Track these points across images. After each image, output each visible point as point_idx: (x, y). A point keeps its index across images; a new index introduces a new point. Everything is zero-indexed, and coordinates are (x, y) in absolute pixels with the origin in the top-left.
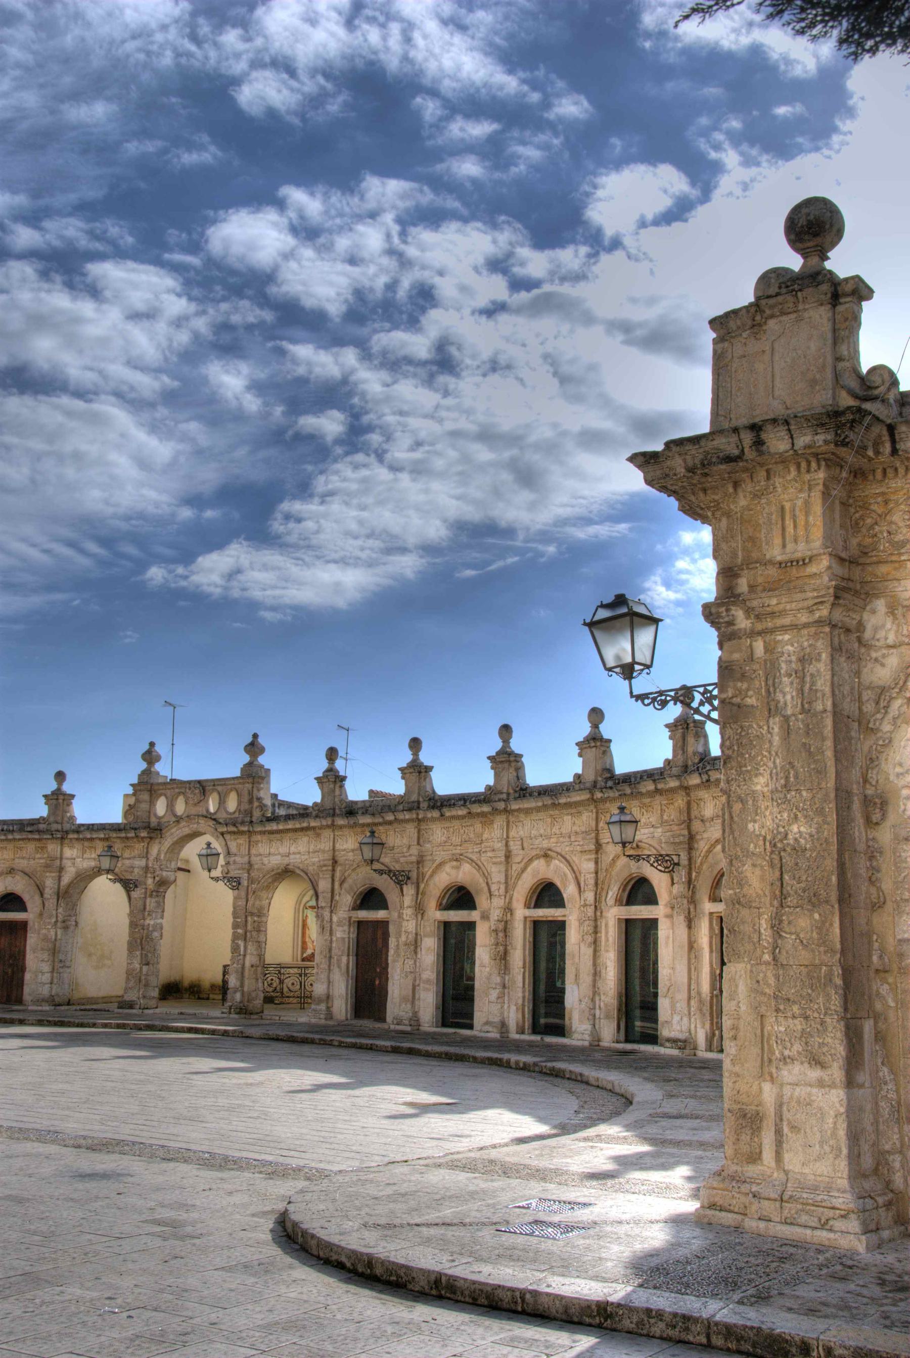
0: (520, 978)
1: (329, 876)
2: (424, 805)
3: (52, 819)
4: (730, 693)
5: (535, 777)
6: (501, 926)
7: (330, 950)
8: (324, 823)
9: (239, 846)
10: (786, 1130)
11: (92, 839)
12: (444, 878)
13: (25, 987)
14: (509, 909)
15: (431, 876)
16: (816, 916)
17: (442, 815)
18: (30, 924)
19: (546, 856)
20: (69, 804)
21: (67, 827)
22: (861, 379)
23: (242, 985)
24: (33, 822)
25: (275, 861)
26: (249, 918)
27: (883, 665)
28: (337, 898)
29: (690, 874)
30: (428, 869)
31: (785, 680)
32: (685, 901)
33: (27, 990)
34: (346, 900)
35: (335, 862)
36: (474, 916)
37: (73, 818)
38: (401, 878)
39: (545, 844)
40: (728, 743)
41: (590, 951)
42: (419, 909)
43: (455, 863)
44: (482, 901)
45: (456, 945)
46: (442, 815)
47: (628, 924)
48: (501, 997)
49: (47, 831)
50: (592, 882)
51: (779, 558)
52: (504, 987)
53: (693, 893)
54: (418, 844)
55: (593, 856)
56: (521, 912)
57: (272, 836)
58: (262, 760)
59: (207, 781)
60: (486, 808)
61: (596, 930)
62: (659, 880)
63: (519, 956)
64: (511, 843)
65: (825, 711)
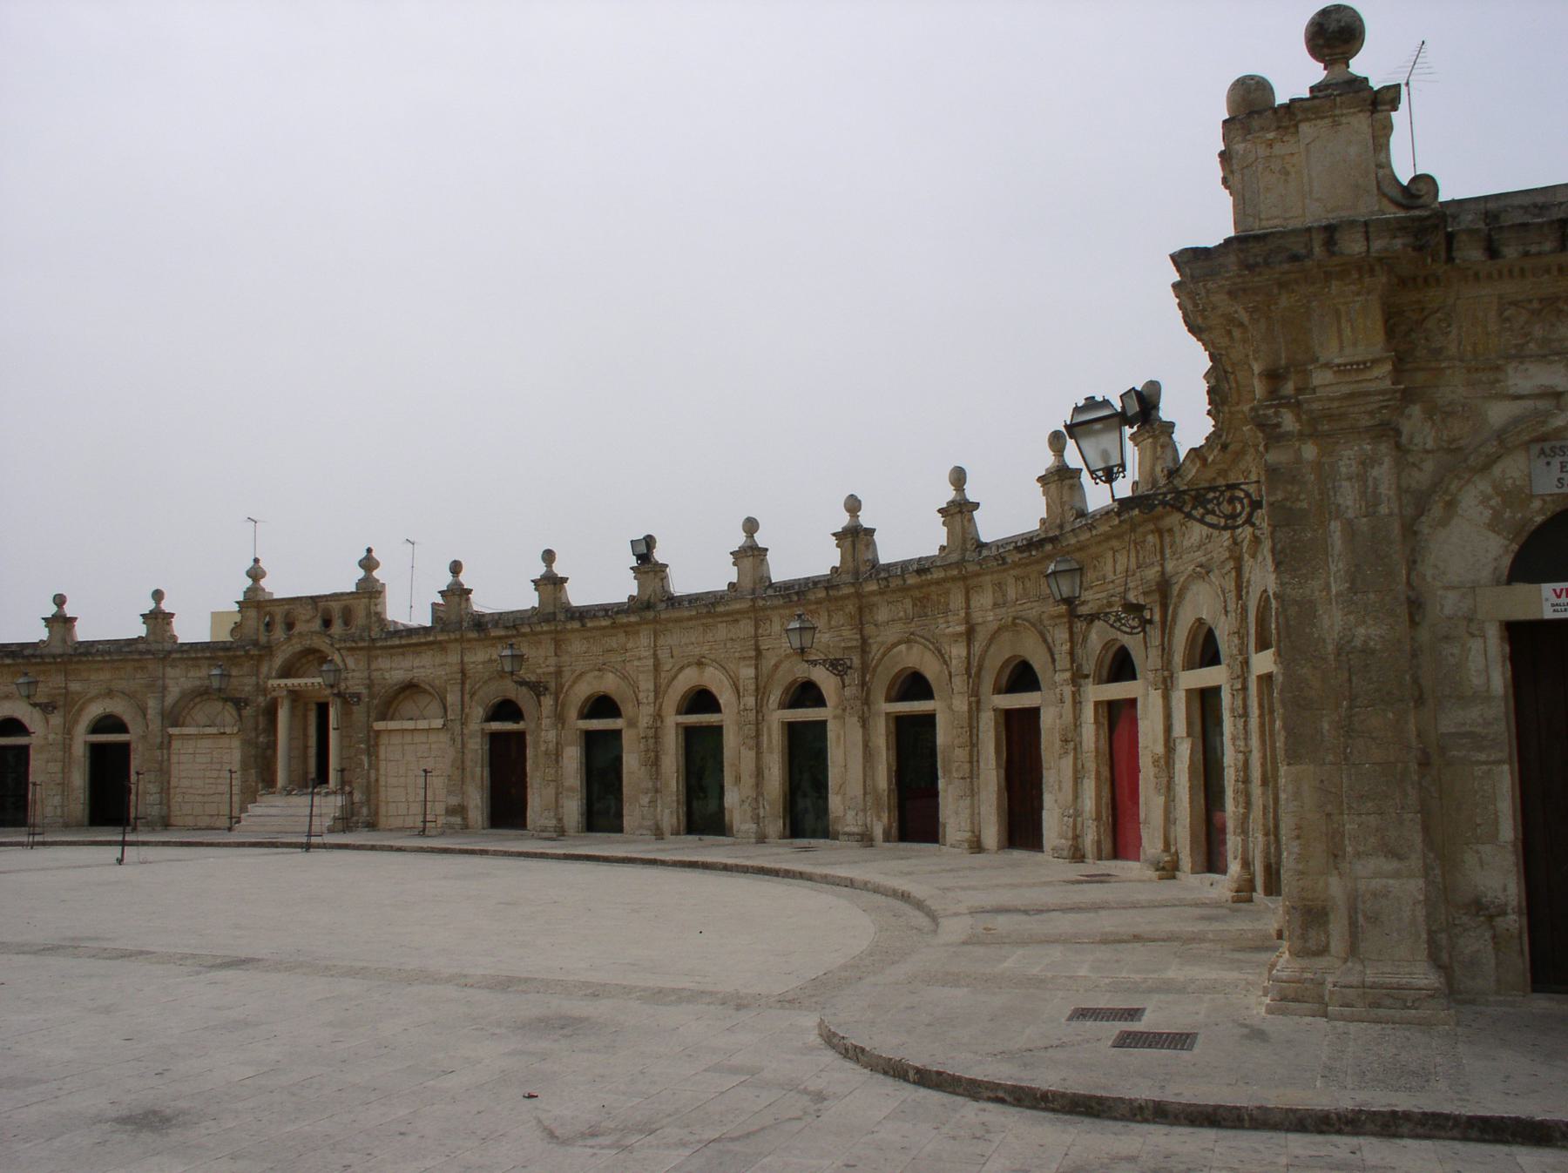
1: (458, 688)
2: (561, 616)
3: (151, 638)
4: (1279, 496)
5: (681, 584)
6: (651, 733)
8: (453, 636)
10: (1361, 920)
11: (196, 659)
12: (583, 690)
14: (658, 716)
15: (571, 687)
16: (1390, 715)
18: (133, 746)
20: (169, 623)
21: (168, 646)
22: (1405, 190)
27: (1420, 470)
29: (863, 676)
30: (567, 676)
31: (1346, 484)
32: (859, 703)
34: (478, 712)
35: (463, 672)
37: (174, 637)
38: (538, 689)
39: (697, 651)
40: (1279, 547)
41: (752, 754)
42: (560, 718)
44: (627, 709)
47: (590, 738)
48: (653, 802)
49: (148, 652)
51: (1337, 361)
52: (657, 791)
53: (868, 694)
58: (376, 574)
61: (758, 735)
62: (825, 680)
63: (671, 762)
65: (1391, 514)
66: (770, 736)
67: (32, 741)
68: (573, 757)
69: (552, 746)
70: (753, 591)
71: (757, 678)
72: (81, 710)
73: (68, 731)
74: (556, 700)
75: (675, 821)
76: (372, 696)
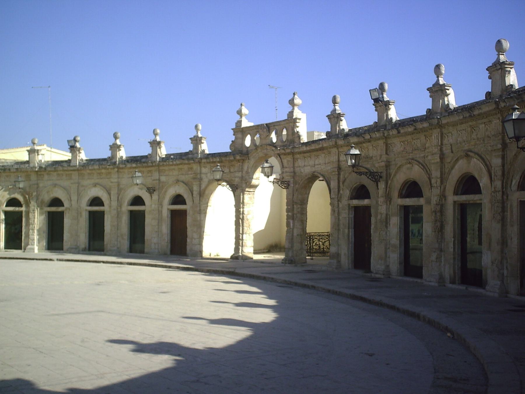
0: (451, 245)
1: (336, 177)
6: (438, 208)
7: (338, 225)
9: (288, 161)
12: (400, 178)
13: (187, 246)
14: (443, 196)
15: (395, 175)
17: (399, 132)
18: (188, 212)
19: (467, 156)
23: (292, 247)
24: (186, 154)
25: (307, 170)
26: (295, 206)
28: (341, 192)
30: (393, 171)
33: (188, 248)
34: (346, 193)
35: (339, 168)
36: (421, 201)
41: (499, 226)
42: (388, 198)
43: (409, 165)
44: (426, 191)
45: (410, 216)
46: (399, 132)
47: (406, 209)
48: (438, 258)
50: (500, 173)
52: (441, 250)
54: (386, 153)
55: (501, 153)
56: (451, 198)
57: (305, 155)
59: (270, 124)
60: (426, 125)
61: (504, 209)
64: (444, 149)
66: (512, 212)
67: (106, 208)
68: (395, 221)
69: (384, 216)
70: (501, 96)
71: (503, 165)
72: (166, 192)
73: (161, 204)
74: (387, 183)
75: (452, 272)
76: (295, 183)
